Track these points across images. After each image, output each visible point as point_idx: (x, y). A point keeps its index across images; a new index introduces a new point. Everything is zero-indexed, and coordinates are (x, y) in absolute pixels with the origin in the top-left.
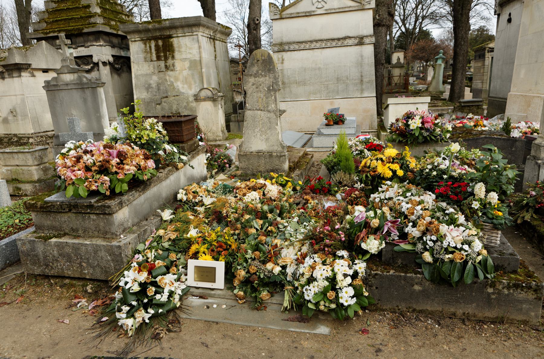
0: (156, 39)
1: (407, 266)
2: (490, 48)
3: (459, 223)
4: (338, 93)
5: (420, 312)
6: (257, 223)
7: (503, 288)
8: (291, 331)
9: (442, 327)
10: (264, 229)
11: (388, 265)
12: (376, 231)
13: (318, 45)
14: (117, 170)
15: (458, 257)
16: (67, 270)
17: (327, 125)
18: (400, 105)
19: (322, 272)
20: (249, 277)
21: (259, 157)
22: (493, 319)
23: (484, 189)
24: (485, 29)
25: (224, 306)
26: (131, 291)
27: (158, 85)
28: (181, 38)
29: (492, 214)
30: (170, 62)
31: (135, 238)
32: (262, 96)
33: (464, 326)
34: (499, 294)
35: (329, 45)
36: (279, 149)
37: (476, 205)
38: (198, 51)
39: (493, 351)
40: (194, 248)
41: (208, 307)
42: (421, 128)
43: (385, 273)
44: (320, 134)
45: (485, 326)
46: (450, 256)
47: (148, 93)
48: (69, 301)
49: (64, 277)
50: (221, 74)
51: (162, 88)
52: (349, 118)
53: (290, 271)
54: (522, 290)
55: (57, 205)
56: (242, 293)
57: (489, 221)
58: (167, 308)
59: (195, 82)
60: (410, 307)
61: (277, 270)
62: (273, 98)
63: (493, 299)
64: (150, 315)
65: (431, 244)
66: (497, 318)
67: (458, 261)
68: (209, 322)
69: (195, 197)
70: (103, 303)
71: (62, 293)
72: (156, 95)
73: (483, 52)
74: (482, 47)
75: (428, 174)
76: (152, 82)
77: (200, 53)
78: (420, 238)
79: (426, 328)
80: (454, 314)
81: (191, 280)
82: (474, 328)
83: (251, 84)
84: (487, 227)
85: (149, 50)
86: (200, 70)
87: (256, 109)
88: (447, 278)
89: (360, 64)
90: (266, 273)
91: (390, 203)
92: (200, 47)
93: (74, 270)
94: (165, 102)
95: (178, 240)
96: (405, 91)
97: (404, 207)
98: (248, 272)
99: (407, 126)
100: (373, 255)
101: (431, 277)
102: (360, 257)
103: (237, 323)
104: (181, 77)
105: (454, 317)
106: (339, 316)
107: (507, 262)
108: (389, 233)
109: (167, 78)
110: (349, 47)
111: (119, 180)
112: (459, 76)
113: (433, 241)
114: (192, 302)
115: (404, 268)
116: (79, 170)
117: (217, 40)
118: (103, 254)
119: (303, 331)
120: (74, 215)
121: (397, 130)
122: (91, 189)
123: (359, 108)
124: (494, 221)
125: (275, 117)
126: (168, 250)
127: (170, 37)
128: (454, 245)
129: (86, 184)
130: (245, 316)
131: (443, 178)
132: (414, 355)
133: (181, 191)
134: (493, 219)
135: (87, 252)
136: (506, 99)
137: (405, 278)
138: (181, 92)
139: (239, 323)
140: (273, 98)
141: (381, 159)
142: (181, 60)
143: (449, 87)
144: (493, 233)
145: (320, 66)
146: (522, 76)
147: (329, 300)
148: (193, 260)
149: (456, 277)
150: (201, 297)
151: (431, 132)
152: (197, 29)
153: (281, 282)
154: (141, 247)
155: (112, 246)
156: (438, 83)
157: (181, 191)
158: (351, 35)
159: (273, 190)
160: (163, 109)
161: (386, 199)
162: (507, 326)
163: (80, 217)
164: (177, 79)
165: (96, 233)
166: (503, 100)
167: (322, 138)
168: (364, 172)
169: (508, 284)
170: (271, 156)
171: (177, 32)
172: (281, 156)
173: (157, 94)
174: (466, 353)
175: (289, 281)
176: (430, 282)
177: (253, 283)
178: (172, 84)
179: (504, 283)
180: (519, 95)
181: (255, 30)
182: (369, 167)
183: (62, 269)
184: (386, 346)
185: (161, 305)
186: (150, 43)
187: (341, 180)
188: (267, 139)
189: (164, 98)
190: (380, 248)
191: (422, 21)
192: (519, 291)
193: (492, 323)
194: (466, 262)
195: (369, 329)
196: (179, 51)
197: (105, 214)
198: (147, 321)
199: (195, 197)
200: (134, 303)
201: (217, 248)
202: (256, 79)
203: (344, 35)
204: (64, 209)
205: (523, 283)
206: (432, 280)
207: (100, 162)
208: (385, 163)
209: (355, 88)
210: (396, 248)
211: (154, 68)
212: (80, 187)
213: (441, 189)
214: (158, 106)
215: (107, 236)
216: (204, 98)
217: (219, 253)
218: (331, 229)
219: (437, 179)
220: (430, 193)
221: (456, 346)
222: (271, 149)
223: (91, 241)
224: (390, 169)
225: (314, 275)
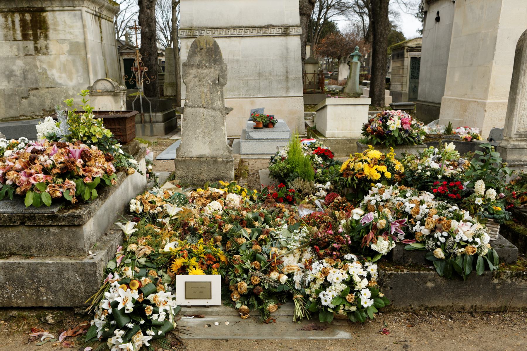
0: (22, 11)
1: (417, 265)
2: (409, 47)
3: (464, 219)
4: (259, 90)
5: (433, 308)
6: (245, 231)
7: (507, 278)
8: (312, 339)
9: (455, 321)
10: (254, 238)
11: (399, 265)
12: (385, 232)
13: (236, 33)
14: (84, 173)
15: (470, 250)
16: (17, 298)
17: (255, 128)
18: (339, 106)
19: (336, 276)
20: (253, 289)
21: (201, 163)
22: (497, 309)
23: (484, 186)
24: (393, 24)
25: (228, 323)
26: (126, 312)
27: (24, 73)
28: (58, 13)
29: (493, 210)
30: (42, 42)
31: (105, 255)
32: (206, 91)
33: (473, 318)
34: (503, 284)
35: (249, 33)
36: (225, 154)
37: (479, 201)
38: (81, 30)
39: (506, 336)
40: (179, 262)
41: (209, 326)
42: (400, 130)
43: (399, 272)
44: (249, 139)
45: (492, 317)
46: (463, 250)
47: (9, 82)
48: (24, 335)
49: (12, 308)
50: (108, 61)
51: (29, 76)
52: (280, 120)
53: (297, 278)
54: (523, 279)
55: (4, 217)
56: (245, 307)
57: (491, 216)
58: (166, 328)
59: (77, 71)
60: (422, 305)
61: (284, 278)
62: (219, 93)
63: (497, 289)
64: (150, 338)
65: (443, 240)
66: (501, 307)
67: (471, 254)
68: (217, 340)
69: (153, 208)
70: (75, 332)
71: (11, 327)
72: (21, 86)
73: (402, 51)
74: (400, 45)
75: (420, 176)
76: (15, 68)
77: (84, 33)
78: (429, 237)
79: (441, 323)
80: (463, 308)
81: (181, 299)
82: (482, 319)
83: (192, 76)
84: (489, 222)
85: (11, 25)
86: (84, 56)
87: (198, 107)
88: (459, 272)
89: (285, 57)
90: (272, 283)
91: (388, 204)
92: (84, 26)
93: (26, 298)
94: (33, 96)
95: (154, 255)
96: (320, 91)
97: (408, 207)
98: (251, 284)
99: (386, 127)
100: (383, 256)
101: (444, 273)
102: (370, 259)
103: (249, 338)
104: (57, 64)
105: (463, 311)
106: (356, 320)
107: (508, 254)
108: (396, 234)
109: (38, 63)
110: (272, 38)
111: (85, 184)
112: (379, 77)
113: (445, 237)
114: (187, 322)
115: (415, 266)
116: (37, 173)
117: (102, 18)
118: (70, 274)
119: (323, 338)
120: (26, 229)
121: (374, 131)
122: (54, 196)
123: (288, 107)
124: (495, 215)
125: (221, 116)
126: (145, 267)
127: (43, 10)
128: (466, 239)
129: (48, 189)
130: (253, 330)
131: (437, 178)
132: (439, 346)
133: (133, 201)
134: (493, 214)
135: (48, 273)
136: (440, 104)
137: (419, 276)
138: (57, 83)
139: (253, 338)
140: (219, 93)
141: (366, 161)
142: (57, 41)
143: (369, 89)
144: (493, 228)
145: (238, 57)
146: (456, 79)
147: (349, 303)
148: (181, 276)
149: (468, 271)
150: (196, 316)
151: (410, 134)
152: (81, 3)
153: (288, 291)
154: (111, 265)
155: (84, 264)
156: (354, 83)
157: (133, 201)
158: (274, 23)
159: (235, 199)
160: (31, 104)
161: (382, 201)
162: (510, 314)
163: (35, 231)
164: (51, 66)
165: (57, 250)
166: (438, 105)
167: (251, 143)
168: (348, 174)
169: (512, 274)
171: (52, 4)
172: (228, 162)
173: (23, 84)
174: (484, 339)
175: (297, 290)
176: (442, 278)
177: (259, 295)
178: (44, 72)
179: (507, 273)
180: (454, 99)
181: (149, 8)
182: (353, 170)
183: (9, 298)
184: (410, 342)
185: (158, 326)
186: (12, 16)
187: (301, 188)
188: (211, 142)
189: (33, 89)
190: (390, 249)
191: (327, 10)
192: (520, 279)
193: (496, 313)
194: (476, 256)
195: (388, 329)
196: (55, 30)
197: (74, 226)
198: (148, 344)
199: (153, 208)
200: (130, 325)
201: (207, 261)
202: (199, 70)
203: (266, 24)
204: (15, 222)
205: (523, 272)
206: (445, 276)
207: (61, 163)
208: (372, 165)
209: (280, 86)
210: (406, 247)
211: (18, 50)
212: (43, 194)
213: (438, 189)
214: (24, 100)
215: (72, 253)
216: (101, 91)
217: (209, 267)
218: (334, 233)
219: (431, 179)
220: (429, 193)
221: (473, 335)
222: (215, 154)
223: (53, 260)
224: (378, 172)
225: (328, 280)
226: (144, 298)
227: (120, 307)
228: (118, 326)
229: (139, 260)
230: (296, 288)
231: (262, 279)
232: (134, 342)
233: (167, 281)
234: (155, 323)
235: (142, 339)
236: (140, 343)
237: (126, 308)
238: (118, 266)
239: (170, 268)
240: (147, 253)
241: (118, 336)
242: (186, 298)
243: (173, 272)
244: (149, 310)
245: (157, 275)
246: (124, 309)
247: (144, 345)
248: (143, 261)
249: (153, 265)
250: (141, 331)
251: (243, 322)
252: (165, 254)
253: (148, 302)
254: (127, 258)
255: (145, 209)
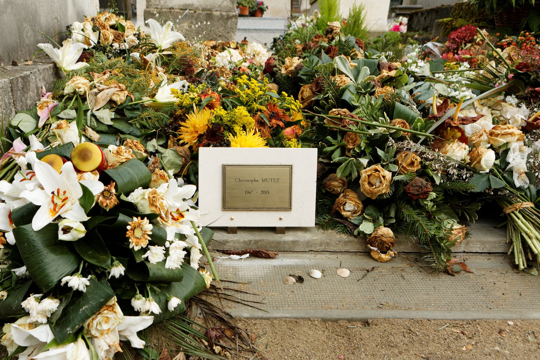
25: (345, 273)
26: (62, 237)
36: (225, 3)
41: (300, 280)
56: (386, 232)
58: (187, 287)
64: (146, 322)
68: (336, 321)
69: (117, 38)
81: (211, 211)
114: (234, 268)
150: (256, 254)
170: (209, 16)
175: (520, 189)
185: (164, 284)
198: (138, 343)
200: (78, 282)
226: (118, 197)
227: (39, 222)
228: (37, 285)
229: (97, 114)
230: (518, 184)
231: (427, 159)
232: (92, 338)
233: (173, 165)
234: (159, 273)
235: (113, 326)
236: (114, 340)
237: (62, 224)
238: (41, 124)
239: (175, 136)
240: (115, 98)
241: (35, 317)
242: (226, 206)
243: (183, 144)
244: (138, 234)
245: (146, 151)
246: (52, 229)
247: (125, 344)
248: (107, 116)
249: (131, 129)
250: (114, 300)
251: (384, 269)
252: (158, 107)
253: (132, 210)
254: (65, 108)
255: (102, 38)
